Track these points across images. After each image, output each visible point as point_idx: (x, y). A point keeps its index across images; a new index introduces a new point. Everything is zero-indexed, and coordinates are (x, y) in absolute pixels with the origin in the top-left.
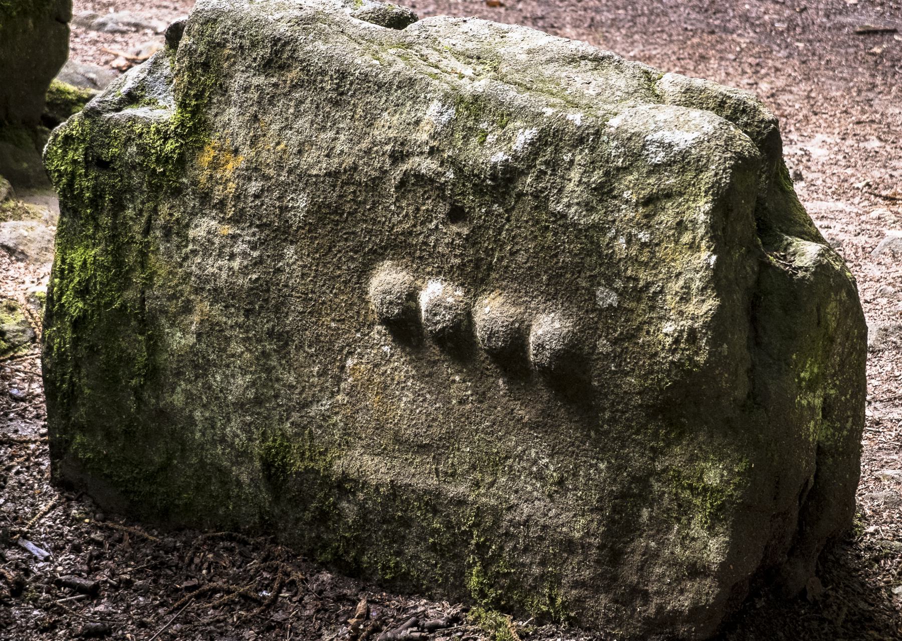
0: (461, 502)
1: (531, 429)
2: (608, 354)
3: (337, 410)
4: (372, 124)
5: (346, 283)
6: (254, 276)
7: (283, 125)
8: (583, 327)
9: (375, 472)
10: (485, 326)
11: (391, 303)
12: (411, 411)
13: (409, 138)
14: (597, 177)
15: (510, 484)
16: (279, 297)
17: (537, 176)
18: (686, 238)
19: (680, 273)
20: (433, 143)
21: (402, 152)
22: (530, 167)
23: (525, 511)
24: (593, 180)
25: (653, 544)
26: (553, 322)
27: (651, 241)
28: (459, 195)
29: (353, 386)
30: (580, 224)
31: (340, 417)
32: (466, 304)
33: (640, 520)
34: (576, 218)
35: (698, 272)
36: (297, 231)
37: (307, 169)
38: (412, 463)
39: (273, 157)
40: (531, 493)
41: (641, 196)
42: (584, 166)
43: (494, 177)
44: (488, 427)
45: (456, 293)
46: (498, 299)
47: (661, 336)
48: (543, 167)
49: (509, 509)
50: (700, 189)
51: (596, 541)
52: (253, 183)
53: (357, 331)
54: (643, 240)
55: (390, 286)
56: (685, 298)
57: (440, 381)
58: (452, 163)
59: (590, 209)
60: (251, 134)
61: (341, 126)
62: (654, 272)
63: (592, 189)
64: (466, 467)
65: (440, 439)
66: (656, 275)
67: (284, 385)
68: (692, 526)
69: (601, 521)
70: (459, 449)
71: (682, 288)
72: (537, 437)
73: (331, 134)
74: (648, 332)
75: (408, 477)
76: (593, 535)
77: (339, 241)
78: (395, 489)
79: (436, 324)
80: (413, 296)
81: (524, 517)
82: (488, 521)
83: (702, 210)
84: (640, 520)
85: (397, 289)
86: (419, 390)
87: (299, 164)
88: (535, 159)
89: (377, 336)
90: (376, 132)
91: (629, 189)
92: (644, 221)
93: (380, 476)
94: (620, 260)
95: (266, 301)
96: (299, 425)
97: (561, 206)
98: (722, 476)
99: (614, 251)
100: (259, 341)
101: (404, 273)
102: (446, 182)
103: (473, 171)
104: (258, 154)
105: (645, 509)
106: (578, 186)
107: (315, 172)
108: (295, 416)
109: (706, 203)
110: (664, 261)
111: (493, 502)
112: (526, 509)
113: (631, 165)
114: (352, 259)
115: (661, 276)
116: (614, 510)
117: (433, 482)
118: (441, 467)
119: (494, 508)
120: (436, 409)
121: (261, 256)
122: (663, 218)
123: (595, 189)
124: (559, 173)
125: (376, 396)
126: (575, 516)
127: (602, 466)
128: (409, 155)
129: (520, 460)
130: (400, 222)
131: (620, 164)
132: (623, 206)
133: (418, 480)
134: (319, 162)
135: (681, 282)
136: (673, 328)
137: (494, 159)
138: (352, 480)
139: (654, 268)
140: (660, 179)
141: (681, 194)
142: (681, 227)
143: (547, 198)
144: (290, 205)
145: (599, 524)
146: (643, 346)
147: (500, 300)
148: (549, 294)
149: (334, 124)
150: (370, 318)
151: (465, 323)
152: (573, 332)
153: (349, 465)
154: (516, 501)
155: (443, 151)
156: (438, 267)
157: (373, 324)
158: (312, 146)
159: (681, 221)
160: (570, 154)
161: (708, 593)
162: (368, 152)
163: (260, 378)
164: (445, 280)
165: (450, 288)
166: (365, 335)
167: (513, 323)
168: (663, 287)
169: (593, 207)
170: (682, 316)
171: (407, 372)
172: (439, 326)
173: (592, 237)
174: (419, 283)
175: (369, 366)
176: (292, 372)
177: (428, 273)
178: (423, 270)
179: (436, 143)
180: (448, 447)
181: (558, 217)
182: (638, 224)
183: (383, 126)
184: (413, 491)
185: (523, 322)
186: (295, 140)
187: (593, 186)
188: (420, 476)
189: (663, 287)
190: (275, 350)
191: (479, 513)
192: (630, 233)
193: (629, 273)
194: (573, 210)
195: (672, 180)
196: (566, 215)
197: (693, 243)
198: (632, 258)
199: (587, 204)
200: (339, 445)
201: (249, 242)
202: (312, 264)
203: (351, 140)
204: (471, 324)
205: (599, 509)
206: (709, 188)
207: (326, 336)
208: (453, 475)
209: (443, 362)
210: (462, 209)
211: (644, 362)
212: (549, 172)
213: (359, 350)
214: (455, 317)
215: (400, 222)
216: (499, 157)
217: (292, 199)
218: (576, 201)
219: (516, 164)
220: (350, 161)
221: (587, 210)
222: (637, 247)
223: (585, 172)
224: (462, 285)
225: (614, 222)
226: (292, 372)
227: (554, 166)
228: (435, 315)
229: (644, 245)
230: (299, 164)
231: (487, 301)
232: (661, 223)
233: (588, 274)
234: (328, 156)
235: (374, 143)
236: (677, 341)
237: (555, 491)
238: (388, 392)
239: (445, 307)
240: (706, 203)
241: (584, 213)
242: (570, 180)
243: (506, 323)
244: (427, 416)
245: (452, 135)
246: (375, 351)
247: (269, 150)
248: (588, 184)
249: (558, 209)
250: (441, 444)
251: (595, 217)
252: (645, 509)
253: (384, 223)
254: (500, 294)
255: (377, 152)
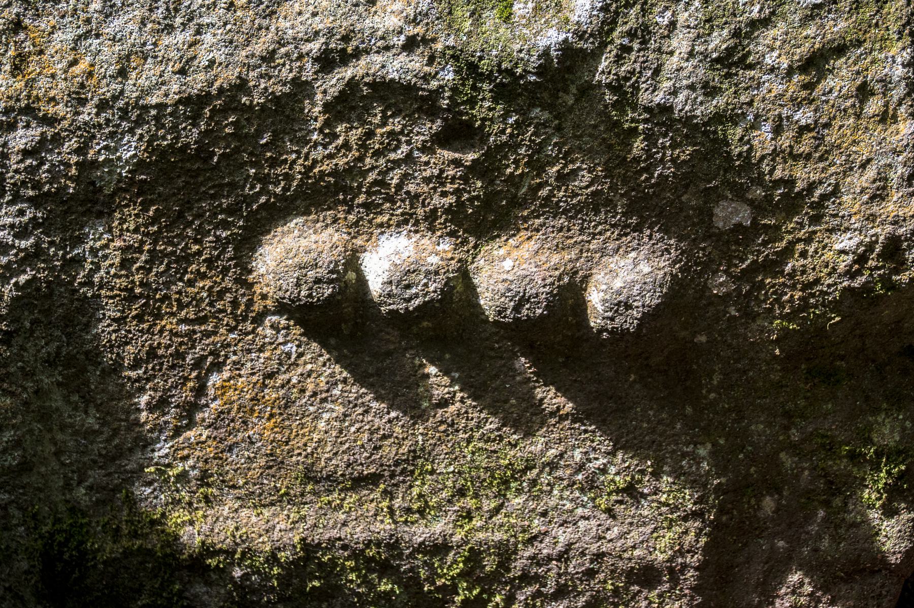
0: (440, 548)
1: (574, 421)
2: (728, 295)
3: (186, 452)
4: (273, 13)
5: (210, 262)
6: (23, 279)
7: (80, 31)
8: (686, 264)
9: (267, 531)
10: (509, 290)
11: (318, 281)
12: (341, 432)
13: (358, 27)
14: (718, 41)
15: (531, 505)
16: (72, 302)
17: (617, 56)
18: (874, 106)
19: (869, 161)
20: (411, 30)
21: (344, 50)
22: (603, 45)
23: (561, 539)
24: (712, 46)
25: (781, 544)
26: (635, 266)
27: (816, 122)
28: (464, 103)
29: (222, 412)
30: (696, 117)
31: (191, 462)
32: (460, 261)
33: (761, 514)
34: (687, 108)
35: (899, 153)
36: (114, 194)
37: (139, 98)
38: (341, 506)
39: (62, 85)
40: (572, 511)
41: (796, 57)
42: (696, 27)
43: (541, 71)
44: (492, 431)
45: (441, 247)
46: (526, 245)
47: (828, 255)
48: (626, 41)
49: (531, 541)
50: (887, 29)
51: (694, 560)
52: (20, 132)
53: (231, 330)
54: (803, 122)
55: (313, 255)
56: (879, 195)
57: (398, 378)
58: (453, 56)
59: (711, 91)
60: (11, 53)
61: (206, 20)
62: (821, 165)
63: (713, 61)
64: (445, 494)
65: (397, 464)
66: (824, 170)
67: (76, 433)
68: (851, 507)
69: (701, 530)
70: (432, 472)
71: (874, 181)
72: (586, 431)
73: (181, 37)
74: (804, 254)
75: (333, 527)
76: (688, 552)
77: (199, 200)
78: (309, 548)
79: (408, 300)
80: (353, 261)
81: (560, 548)
82: (489, 564)
83: (899, 60)
84: (761, 514)
85: (326, 258)
86: (356, 399)
87: (122, 92)
88: (612, 30)
89: (269, 332)
90: (283, 24)
91: (773, 50)
92: (804, 94)
93: (276, 535)
94: (763, 158)
95: (47, 312)
96: (104, 488)
97: (661, 94)
98: (904, 429)
99: (752, 146)
100: (28, 374)
101: (330, 230)
102: (441, 87)
103: (499, 65)
104: (30, 84)
105: (768, 498)
106: (687, 60)
107: (154, 100)
108: (95, 476)
109: (904, 49)
110: (839, 147)
111: (499, 536)
112: (563, 536)
113: (773, 13)
114: (225, 225)
115: (833, 169)
116: (721, 511)
117: (383, 527)
118: (397, 503)
119: (500, 545)
120: (390, 421)
121: (37, 245)
122: (832, 84)
123: (718, 60)
124: (652, 45)
125: (269, 419)
126: (655, 530)
127: (702, 452)
128: (357, 54)
129: (551, 470)
130: (330, 156)
131: (755, 15)
132: (765, 78)
133: (354, 528)
134: (163, 83)
135: (871, 172)
136: (856, 240)
137: (542, 42)
138: (221, 551)
139: (821, 159)
140: (822, 26)
141: (859, 43)
142: (864, 92)
143: (636, 88)
144: (102, 158)
145: (698, 535)
146: (792, 275)
147: (532, 245)
148: (628, 226)
149: (190, 20)
150: (257, 307)
151: (460, 288)
152: (671, 274)
153: (212, 530)
154: (543, 528)
155: (434, 40)
156: (402, 214)
157: (265, 313)
158: (146, 59)
159: (864, 85)
160: (668, 14)
161: (880, 595)
162: (269, 58)
163: (31, 431)
164: (416, 232)
165: (425, 241)
166: (247, 334)
167: (560, 278)
168: (837, 185)
169: (714, 88)
170: (873, 221)
171: (332, 375)
172: (417, 302)
173: (715, 132)
174: (359, 242)
175: (255, 378)
176: (92, 411)
177: (381, 225)
178: (370, 222)
179: (419, 30)
180: (412, 472)
181: (656, 111)
182: (793, 99)
183: (300, 13)
184: (345, 547)
185: (576, 272)
186: (109, 53)
187: (714, 55)
188: (360, 522)
189: (837, 185)
190: (59, 384)
191: (474, 557)
192: (780, 116)
193: (778, 174)
194: (681, 97)
195: (842, 25)
196: (671, 106)
197: (886, 112)
198: (783, 151)
199: (705, 85)
200: (190, 504)
201: (12, 226)
202: (142, 243)
203: (231, 42)
204: (471, 288)
205: (695, 515)
206: (904, 26)
207: (168, 347)
208: (421, 512)
209: (406, 350)
210: (469, 125)
211: (792, 296)
212: (636, 46)
213: (234, 358)
214: (446, 284)
215: (330, 156)
216: (552, 37)
217: (106, 148)
218: (685, 82)
219: (581, 45)
220: (229, 76)
221: (705, 94)
222: (791, 134)
223: (698, 37)
224: (452, 234)
225: (750, 104)
226: (92, 411)
227: (643, 36)
228: (408, 287)
229: (803, 129)
230: (122, 92)
231: (502, 252)
232: (830, 91)
233: (702, 187)
234: (183, 72)
235: (281, 43)
236: (861, 259)
237: (617, 502)
238: (293, 409)
239: (428, 273)
240: (904, 49)
241: (700, 99)
242: (671, 53)
243: (548, 281)
244: (372, 433)
245: (450, 13)
246: (267, 354)
247: (53, 76)
248: (705, 55)
249: (657, 100)
250: (399, 469)
251: (720, 101)
252: (768, 498)
253: (294, 162)
254: (529, 238)
255: (287, 55)
